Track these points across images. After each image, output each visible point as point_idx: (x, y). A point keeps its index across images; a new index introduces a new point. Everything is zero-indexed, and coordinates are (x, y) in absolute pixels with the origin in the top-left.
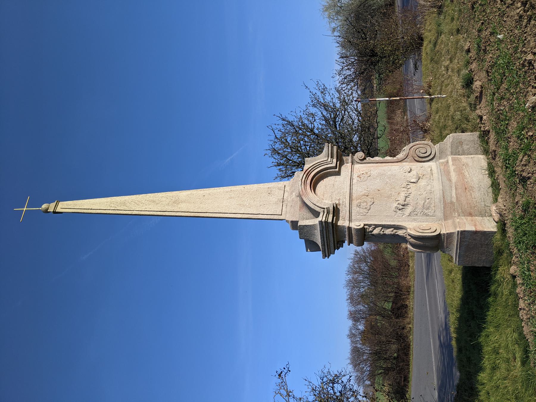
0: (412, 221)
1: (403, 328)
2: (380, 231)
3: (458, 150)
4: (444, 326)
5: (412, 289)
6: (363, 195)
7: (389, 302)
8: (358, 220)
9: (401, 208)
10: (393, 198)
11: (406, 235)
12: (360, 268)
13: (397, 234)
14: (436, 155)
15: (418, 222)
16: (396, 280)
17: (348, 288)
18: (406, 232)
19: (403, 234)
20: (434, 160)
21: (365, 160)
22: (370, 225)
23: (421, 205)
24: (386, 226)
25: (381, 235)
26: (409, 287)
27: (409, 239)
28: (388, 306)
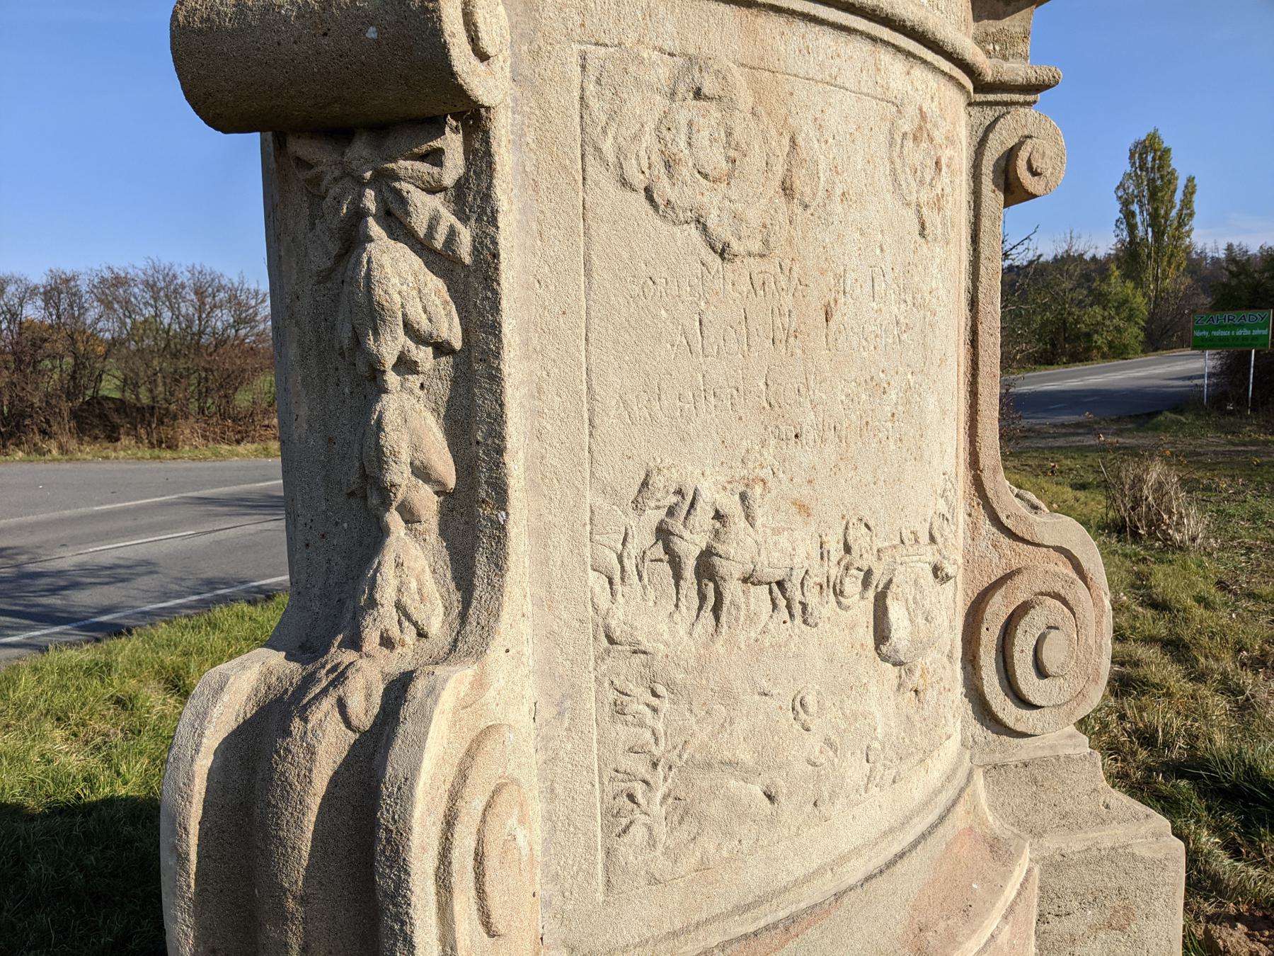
0: (547, 671)
1: (43, 432)
2: (409, 329)
3: (1075, 904)
4: (32, 568)
5: (168, 454)
6: (793, 141)
7: (124, 391)
8: (536, 54)
9: (679, 546)
10: (769, 455)
11: (387, 642)
12: (215, 306)
13: (382, 532)
14: (1017, 741)
15: (547, 739)
16: (194, 407)
17: (150, 272)
18: (421, 634)
19: (399, 606)
20: (977, 729)
21: (1001, 196)
22: (487, 197)
24: (484, 403)
25: (358, 342)
26: (172, 446)
27: (342, 705)
28: (109, 388)
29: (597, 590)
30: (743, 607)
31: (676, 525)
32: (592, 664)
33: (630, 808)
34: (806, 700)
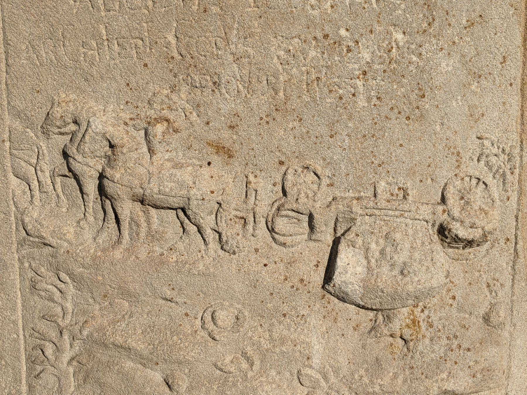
9: (77, 167)
23: (114, 322)
29: (18, 192)
30: (144, 225)
31: (72, 151)
32: (15, 246)
33: (42, 359)
34: (217, 314)
